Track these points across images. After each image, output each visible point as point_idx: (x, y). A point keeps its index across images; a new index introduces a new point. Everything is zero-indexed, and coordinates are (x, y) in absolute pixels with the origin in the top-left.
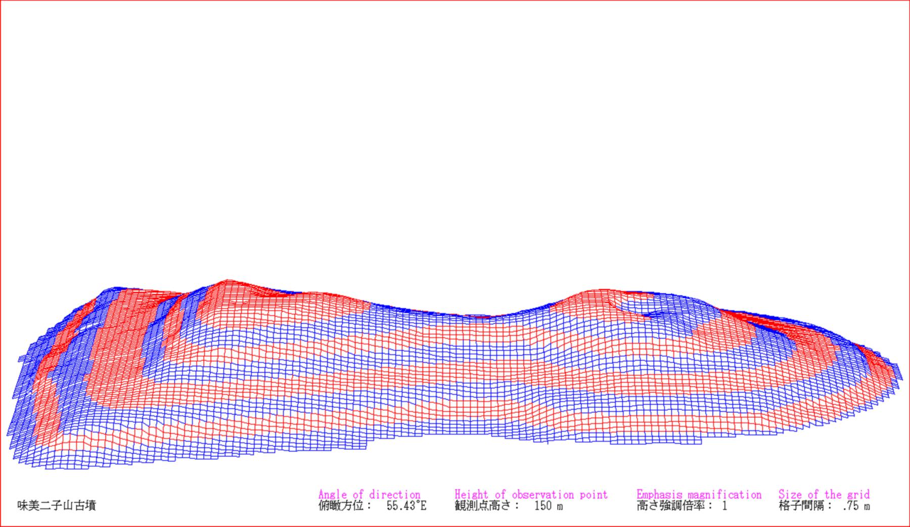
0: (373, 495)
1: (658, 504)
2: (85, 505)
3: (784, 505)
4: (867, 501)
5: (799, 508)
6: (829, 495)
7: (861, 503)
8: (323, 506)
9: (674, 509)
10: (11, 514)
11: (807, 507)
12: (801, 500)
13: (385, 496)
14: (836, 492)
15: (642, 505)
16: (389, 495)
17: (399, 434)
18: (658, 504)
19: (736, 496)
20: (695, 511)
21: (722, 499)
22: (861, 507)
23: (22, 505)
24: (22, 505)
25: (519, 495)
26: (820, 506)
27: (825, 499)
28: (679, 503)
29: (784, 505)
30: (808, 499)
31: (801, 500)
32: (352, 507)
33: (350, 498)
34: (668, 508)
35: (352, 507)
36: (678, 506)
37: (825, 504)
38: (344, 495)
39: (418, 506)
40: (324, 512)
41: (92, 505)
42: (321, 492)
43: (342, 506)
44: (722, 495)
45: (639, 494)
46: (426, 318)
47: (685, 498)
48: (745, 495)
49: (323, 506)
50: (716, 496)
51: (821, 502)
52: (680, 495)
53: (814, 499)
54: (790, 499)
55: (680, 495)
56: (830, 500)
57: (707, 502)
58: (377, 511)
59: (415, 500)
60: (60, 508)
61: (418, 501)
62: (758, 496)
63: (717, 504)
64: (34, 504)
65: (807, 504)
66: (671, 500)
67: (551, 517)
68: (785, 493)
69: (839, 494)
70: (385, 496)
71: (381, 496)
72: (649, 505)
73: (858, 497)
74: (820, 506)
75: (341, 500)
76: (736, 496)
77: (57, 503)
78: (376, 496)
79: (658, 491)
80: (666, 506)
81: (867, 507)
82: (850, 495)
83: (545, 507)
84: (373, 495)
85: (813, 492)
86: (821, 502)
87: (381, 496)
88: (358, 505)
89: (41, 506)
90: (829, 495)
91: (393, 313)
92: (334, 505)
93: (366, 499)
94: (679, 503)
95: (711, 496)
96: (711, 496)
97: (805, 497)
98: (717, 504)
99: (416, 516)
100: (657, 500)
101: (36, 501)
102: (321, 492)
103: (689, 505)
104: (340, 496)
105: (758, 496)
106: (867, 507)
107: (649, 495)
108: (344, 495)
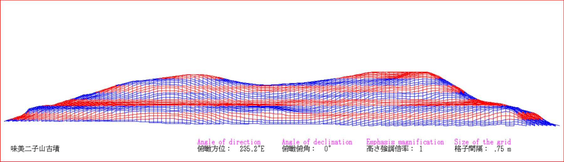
0: (231, 142)
1: (380, 148)
2: (53, 149)
3: (458, 149)
4: (509, 146)
5: (467, 150)
6: (486, 142)
7: (506, 147)
8: (200, 149)
9: (389, 151)
10: (7, 154)
11: (472, 150)
12: (468, 145)
13: (239, 143)
14: (490, 140)
15: (370, 149)
16: (241, 142)
17: (517, 123)
18: (380, 148)
19: (428, 143)
20: (403, 152)
21: (420, 145)
22: (506, 150)
23: (14, 149)
24: (14, 149)
25: (317, 142)
26: (480, 149)
27: (483, 145)
28: (393, 147)
29: (458, 149)
30: (473, 145)
31: (468, 145)
32: (218, 150)
33: (217, 145)
34: (386, 150)
35: (218, 150)
36: (392, 149)
37: (483, 148)
38: (213, 142)
39: (259, 149)
40: (285, 153)
41: (57, 148)
42: (284, 140)
43: (212, 149)
44: (419, 143)
45: (368, 142)
46: (164, 82)
47: (396, 144)
48: (342, 142)
49: (200, 149)
50: (416, 143)
51: (481, 147)
52: (393, 142)
53: (476, 145)
54: (461, 145)
55: (393, 142)
56: (486, 145)
57: (410, 146)
58: (233, 153)
59: (257, 145)
60: (37, 150)
61: (259, 146)
62: (441, 143)
63: (416, 147)
64: (21, 148)
65: (472, 148)
66: (388, 145)
67: (246, 156)
68: (458, 141)
69: (492, 142)
70: (239, 143)
71: (236, 143)
72: (374, 148)
73: (504, 143)
74: (480, 149)
75: (212, 145)
76: (428, 143)
77: (36, 147)
78: (233, 143)
79: (380, 140)
80: (385, 149)
81: (509, 150)
82: (498, 142)
83: (247, 149)
84: (231, 142)
85: (476, 141)
86: (481, 147)
87: (236, 143)
88: (222, 149)
89: (26, 149)
90: (486, 142)
91: (238, 85)
92: (207, 149)
93: (227, 145)
94: (393, 147)
95: (413, 143)
96: (413, 143)
97: (470, 144)
98: (416, 147)
99: (258, 156)
100: (379, 145)
101: (22, 146)
102: (199, 140)
103: (399, 148)
104: (211, 143)
105: (441, 143)
106: (509, 150)
107: (374, 143)
108: (213, 142)
